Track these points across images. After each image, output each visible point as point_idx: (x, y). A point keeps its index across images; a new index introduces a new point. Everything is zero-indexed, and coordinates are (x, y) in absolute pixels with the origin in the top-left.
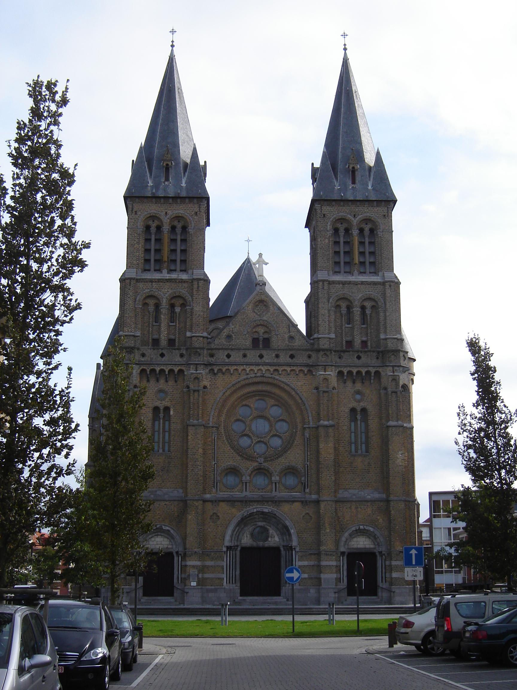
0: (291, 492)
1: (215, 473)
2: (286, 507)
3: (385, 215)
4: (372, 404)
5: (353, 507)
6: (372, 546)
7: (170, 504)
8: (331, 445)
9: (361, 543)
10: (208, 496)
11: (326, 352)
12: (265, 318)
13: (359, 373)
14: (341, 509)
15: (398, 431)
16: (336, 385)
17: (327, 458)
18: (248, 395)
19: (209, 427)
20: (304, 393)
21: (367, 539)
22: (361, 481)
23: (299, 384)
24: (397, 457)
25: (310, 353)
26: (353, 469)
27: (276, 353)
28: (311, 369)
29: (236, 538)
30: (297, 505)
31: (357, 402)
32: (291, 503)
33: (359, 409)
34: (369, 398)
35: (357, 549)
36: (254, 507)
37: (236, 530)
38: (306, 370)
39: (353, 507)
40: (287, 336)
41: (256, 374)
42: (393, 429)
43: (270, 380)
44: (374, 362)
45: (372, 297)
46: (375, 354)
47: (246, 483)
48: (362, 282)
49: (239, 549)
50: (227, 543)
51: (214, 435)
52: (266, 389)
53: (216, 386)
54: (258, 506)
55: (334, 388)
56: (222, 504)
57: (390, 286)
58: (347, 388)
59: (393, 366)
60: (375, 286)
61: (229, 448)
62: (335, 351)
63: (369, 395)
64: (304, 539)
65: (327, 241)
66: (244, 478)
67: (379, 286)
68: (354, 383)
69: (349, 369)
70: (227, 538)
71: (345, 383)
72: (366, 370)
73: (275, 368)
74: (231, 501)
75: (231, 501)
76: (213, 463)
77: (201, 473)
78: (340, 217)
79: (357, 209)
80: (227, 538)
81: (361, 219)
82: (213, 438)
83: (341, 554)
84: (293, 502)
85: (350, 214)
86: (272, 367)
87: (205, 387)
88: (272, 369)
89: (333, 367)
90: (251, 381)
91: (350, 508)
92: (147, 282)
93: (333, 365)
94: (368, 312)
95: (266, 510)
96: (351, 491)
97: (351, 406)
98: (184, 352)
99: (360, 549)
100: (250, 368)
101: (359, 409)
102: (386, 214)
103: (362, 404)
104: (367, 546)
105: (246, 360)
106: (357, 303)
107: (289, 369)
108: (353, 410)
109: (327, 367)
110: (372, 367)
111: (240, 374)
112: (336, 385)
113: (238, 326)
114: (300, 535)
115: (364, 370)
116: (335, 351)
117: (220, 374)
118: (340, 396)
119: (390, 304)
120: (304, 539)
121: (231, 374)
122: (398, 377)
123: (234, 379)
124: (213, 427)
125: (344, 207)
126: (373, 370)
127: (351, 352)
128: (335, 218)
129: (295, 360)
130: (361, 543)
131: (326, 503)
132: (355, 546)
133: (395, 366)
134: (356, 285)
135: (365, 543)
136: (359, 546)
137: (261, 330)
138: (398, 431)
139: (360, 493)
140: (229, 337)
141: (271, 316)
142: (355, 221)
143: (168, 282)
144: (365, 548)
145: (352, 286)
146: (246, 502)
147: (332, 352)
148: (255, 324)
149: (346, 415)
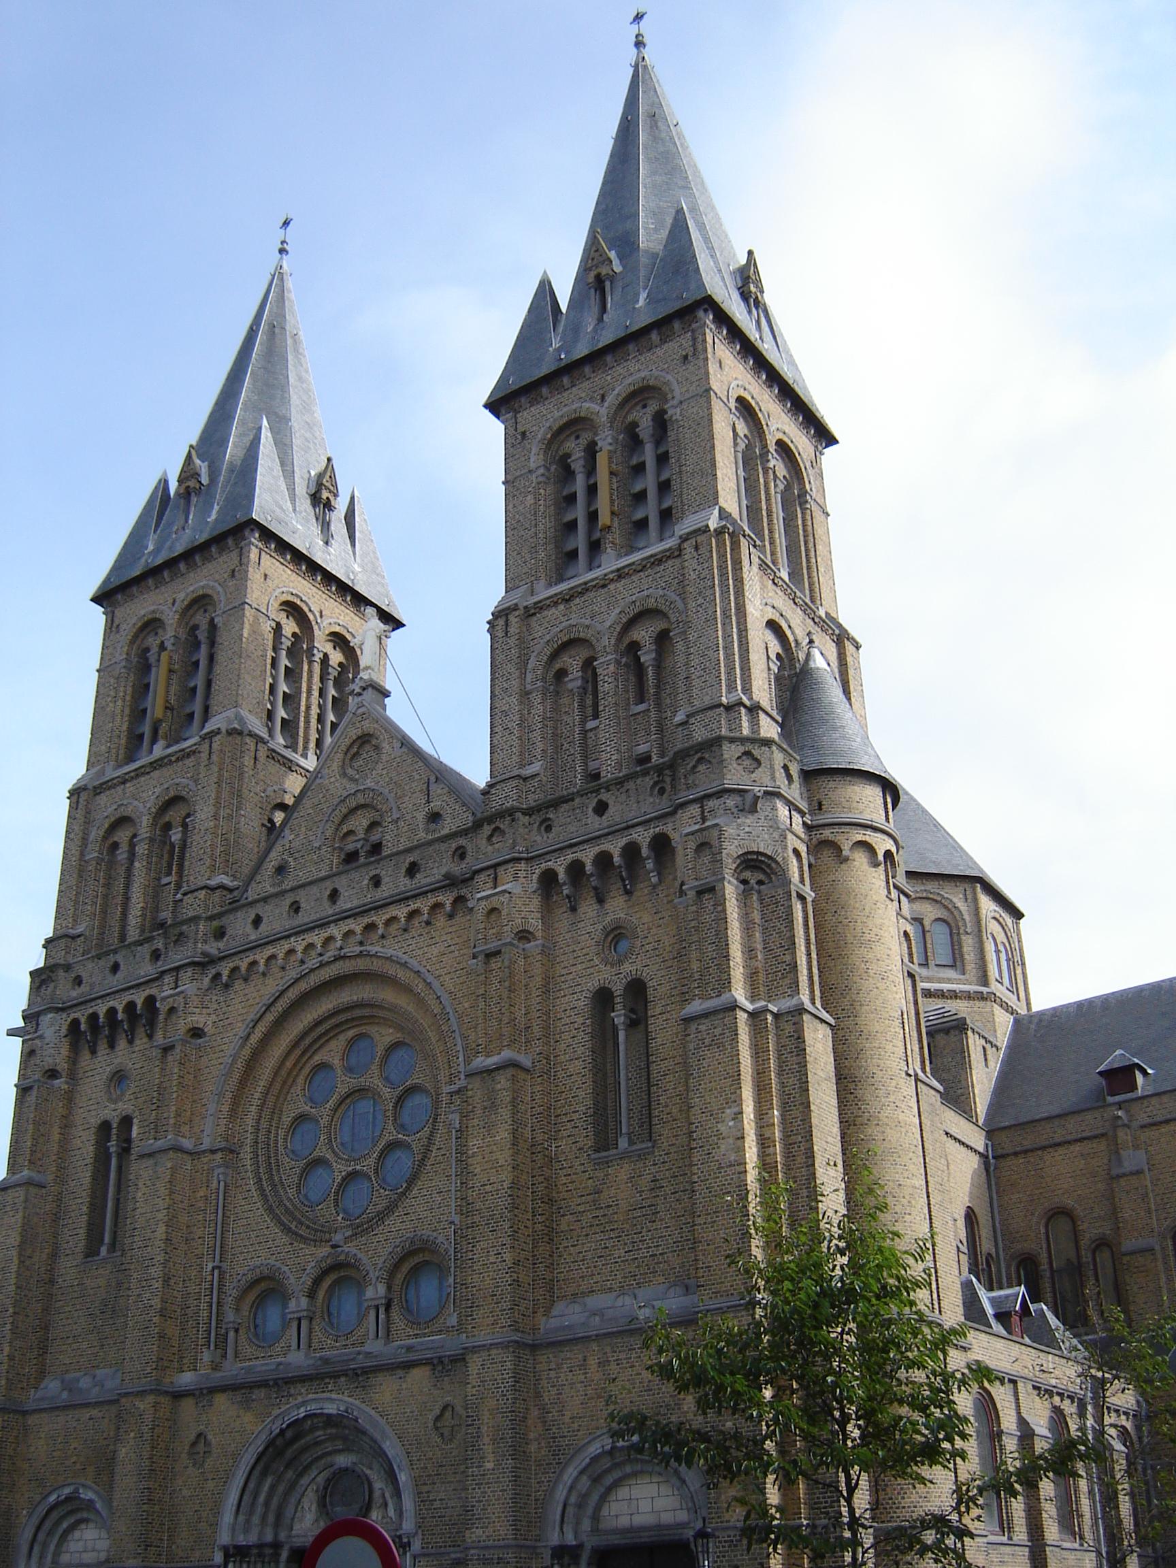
0: (424, 1335)
1: (215, 1300)
2: (386, 1389)
3: (686, 357)
4: (659, 960)
5: (593, 1362)
6: (683, 1516)
7: (100, 1415)
8: (503, 1134)
9: (645, 1506)
10: (187, 1379)
11: (497, 824)
12: (369, 783)
13: (603, 860)
14: (553, 1374)
15: (718, 1031)
16: (535, 923)
17: (488, 1188)
18: (321, 1029)
19: (204, 1152)
20: (447, 978)
21: (665, 1489)
22: (630, 1257)
23: (435, 951)
24: (719, 1134)
25: (462, 841)
26: (601, 1212)
27: (372, 874)
28: (463, 892)
29: (271, 1518)
30: (419, 1375)
31: (612, 965)
32: (400, 1373)
33: (618, 989)
34: (650, 939)
35: (631, 1530)
36: (300, 1399)
37: (266, 1488)
38: (447, 899)
39: (593, 1362)
40: (421, 816)
41: (321, 955)
42: (702, 1028)
43: (362, 965)
44: (651, 805)
45: (651, 604)
46: (649, 781)
47: (299, 1319)
48: (618, 570)
49: (284, 1555)
50: (225, 1538)
51: (215, 1174)
52: (360, 996)
53: (227, 1022)
54: (310, 1396)
55: (524, 935)
56: (221, 1400)
57: (697, 548)
58: (580, 925)
59: (701, 800)
60: (658, 569)
61: (262, 1211)
62: (528, 812)
63: (649, 929)
64: (437, 1504)
65: (530, 500)
66: (292, 1305)
67: (670, 562)
68: (601, 901)
69: (570, 857)
70: (227, 1517)
71: (573, 909)
72: (623, 842)
73: (366, 920)
74: (240, 1388)
75: (240, 1388)
76: (210, 1266)
77: (156, 1302)
78: (565, 419)
79: (609, 377)
80: (227, 1517)
81: (620, 399)
82: (214, 1185)
83: (553, 1557)
84: (408, 1366)
85: (592, 399)
86: (359, 919)
87: (197, 1033)
88: (357, 926)
89: (523, 865)
90: (314, 980)
91: (583, 1365)
92: (114, 786)
93: (521, 859)
94: (647, 657)
95: (331, 1409)
96: (594, 1302)
97: (593, 984)
98: (160, 946)
99: (642, 1529)
100: (305, 943)
101: (618, 989)
102: (690, 351)
103: (627, 967)
104: (667, 1518)
105: (302, 918)
106: (606, 643)
107: (401, 912)
108: (603, 998)
109: (501, 870)
110: (640, 829)
111: (283, 968)
112: (535, 923)
113: (303, 829)
114: (425, 1488)
115: (615, 847)
116: (528, 812)
117: (238, 985)
118: (562, 958)
119: (701, 601)
120: (437, 1504)
121: (264, 974)
122: (715, 833)
123: (271, 986)
124: (213, 1152)
125: (574, 389)
126: (643, 837)
127: (577, 801)
128: (550, 428)
129: (421, 879)
130: (645, 1506)
131: (484, 1354)
132: (624, 1521)
133: (708, 796)
134: (604, 586)
135: (660, 1504)
136: (638, 1520)
137: (360, 823)
138: (718, 1031)
139: (619, 1303)
140: (281, 870)
141: (385, 772)
142: (603, 411)
143: (155, 769)
144: (660, 1527)
145: (592, 594)
146: (281, 1383)
147: (518, 815)
148: (344, 811)
149: (580, 1020)
